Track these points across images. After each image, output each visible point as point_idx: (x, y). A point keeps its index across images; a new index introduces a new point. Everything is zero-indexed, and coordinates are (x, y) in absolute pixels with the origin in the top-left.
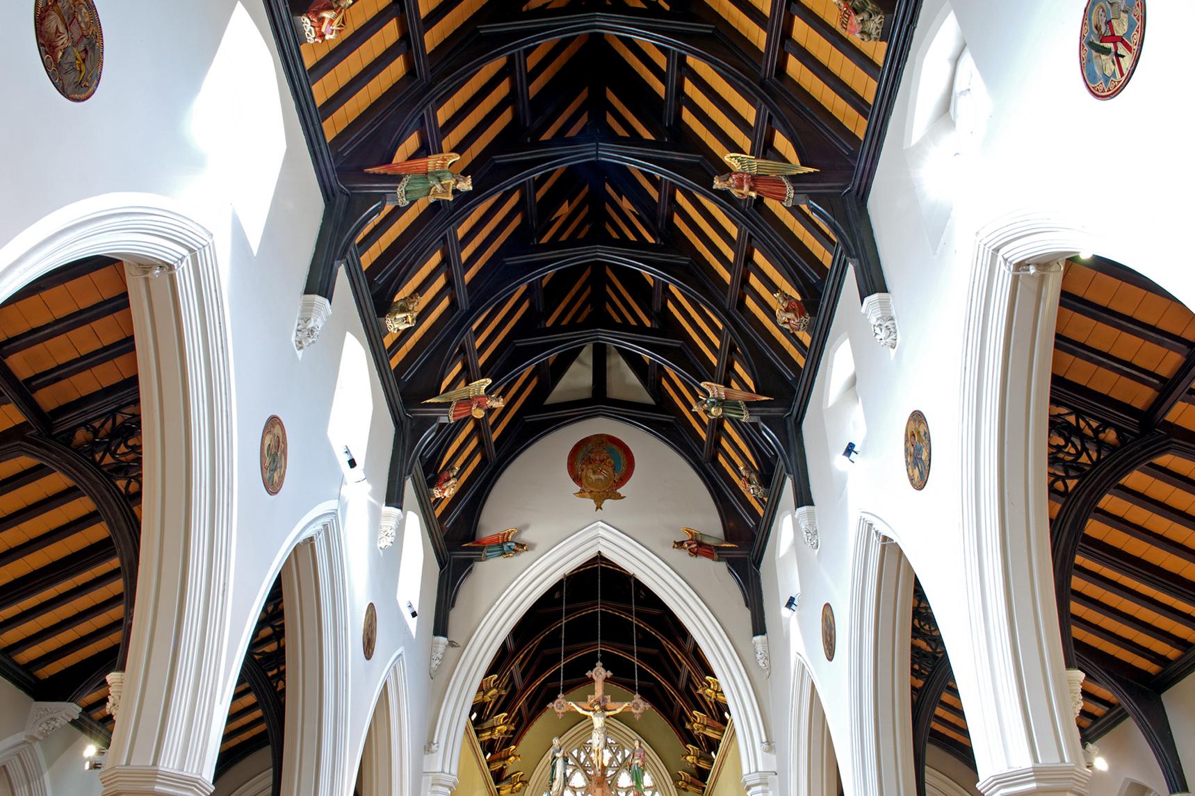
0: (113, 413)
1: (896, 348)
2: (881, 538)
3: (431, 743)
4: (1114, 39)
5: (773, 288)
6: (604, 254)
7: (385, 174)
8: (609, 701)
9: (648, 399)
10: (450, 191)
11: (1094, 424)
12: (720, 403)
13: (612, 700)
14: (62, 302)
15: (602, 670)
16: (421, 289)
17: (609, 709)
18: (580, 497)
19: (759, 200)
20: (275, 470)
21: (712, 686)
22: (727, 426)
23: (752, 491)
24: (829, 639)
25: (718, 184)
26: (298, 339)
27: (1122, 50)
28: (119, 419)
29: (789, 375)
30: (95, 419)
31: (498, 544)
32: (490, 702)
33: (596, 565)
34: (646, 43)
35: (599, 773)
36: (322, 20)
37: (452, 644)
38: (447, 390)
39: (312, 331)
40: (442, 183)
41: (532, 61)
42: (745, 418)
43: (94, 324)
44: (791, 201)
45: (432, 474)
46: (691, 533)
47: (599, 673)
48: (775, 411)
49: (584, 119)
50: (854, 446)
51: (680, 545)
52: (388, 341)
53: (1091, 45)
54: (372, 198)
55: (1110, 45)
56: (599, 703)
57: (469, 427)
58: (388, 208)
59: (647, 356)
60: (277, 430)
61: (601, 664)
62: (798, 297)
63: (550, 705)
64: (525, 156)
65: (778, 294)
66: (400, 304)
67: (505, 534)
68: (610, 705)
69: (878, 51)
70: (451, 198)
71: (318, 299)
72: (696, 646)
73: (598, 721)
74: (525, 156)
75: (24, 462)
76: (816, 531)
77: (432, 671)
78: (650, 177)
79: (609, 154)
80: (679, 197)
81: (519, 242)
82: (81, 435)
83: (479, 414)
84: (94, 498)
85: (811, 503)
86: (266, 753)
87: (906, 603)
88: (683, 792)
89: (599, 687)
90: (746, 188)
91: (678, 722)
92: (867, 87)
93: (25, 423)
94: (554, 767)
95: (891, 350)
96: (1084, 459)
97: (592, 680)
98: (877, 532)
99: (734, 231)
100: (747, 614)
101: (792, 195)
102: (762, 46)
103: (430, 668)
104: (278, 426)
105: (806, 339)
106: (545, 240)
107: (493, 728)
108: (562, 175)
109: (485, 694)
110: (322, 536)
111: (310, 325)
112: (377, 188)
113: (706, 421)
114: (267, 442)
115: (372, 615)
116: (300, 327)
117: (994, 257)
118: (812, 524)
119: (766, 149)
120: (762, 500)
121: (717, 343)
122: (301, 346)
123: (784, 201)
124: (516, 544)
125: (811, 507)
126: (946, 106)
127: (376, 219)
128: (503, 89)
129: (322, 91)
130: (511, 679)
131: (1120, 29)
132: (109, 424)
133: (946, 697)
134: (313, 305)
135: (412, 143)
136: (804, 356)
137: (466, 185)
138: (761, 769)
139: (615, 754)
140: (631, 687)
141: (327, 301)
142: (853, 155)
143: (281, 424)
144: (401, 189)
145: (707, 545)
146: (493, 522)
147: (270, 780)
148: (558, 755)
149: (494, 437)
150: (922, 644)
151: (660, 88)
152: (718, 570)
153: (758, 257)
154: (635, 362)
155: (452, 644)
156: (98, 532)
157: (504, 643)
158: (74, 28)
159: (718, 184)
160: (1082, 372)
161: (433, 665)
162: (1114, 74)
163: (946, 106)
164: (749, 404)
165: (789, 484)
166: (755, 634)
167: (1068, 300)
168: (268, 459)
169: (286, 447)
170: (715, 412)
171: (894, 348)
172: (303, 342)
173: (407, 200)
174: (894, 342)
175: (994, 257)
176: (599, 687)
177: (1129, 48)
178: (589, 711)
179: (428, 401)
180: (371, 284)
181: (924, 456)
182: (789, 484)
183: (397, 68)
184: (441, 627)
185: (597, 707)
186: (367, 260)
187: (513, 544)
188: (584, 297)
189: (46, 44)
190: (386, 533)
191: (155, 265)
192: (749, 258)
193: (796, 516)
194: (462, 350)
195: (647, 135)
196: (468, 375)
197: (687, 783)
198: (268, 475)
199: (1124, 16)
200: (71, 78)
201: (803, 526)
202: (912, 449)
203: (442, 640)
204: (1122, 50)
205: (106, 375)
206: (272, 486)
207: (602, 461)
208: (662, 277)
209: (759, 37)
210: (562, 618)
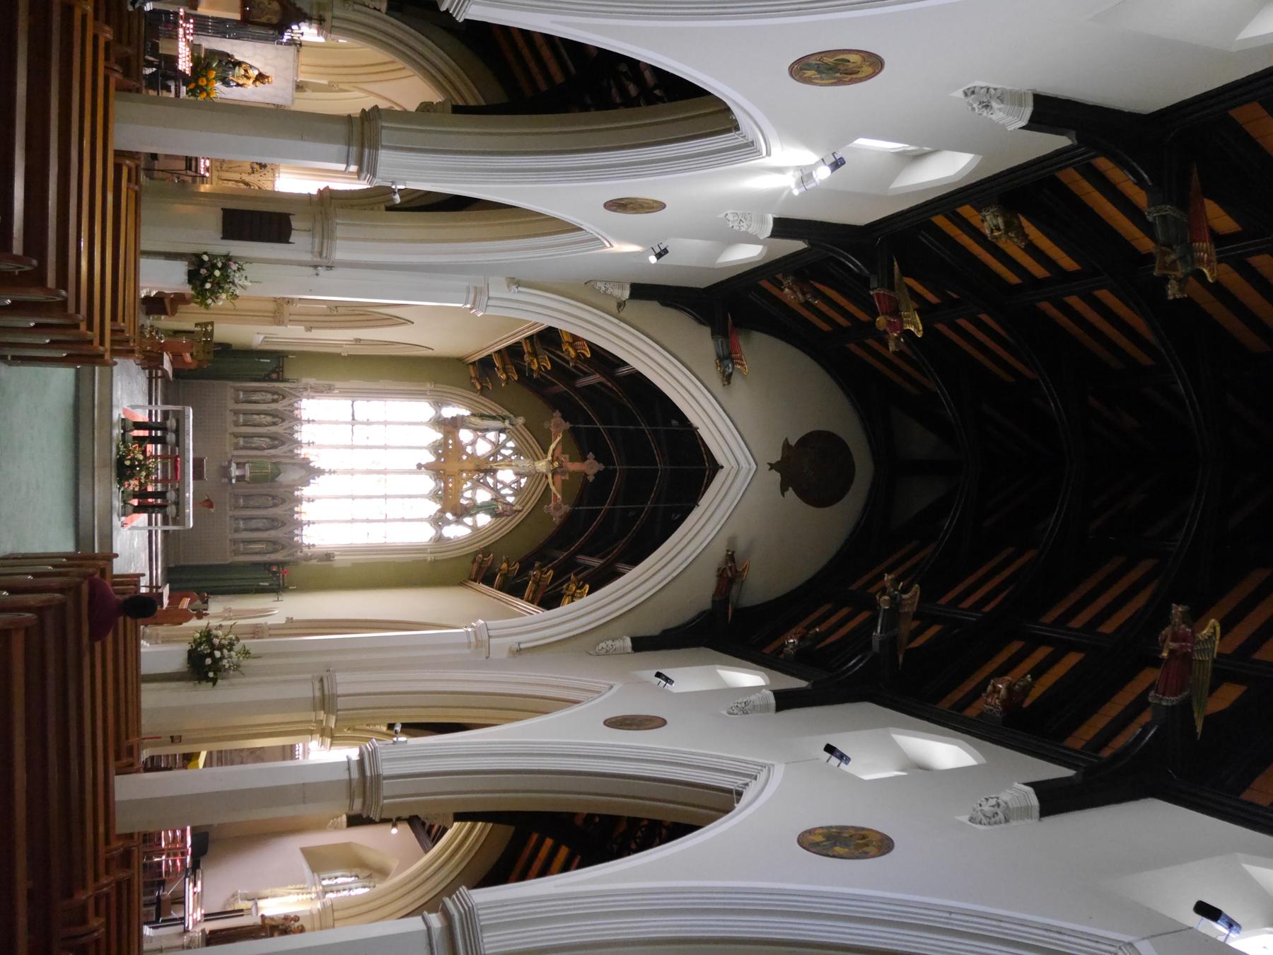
1: (969, 823)
2: (740, 789)
3: (519, 284)
5: (1038, 672)
8: (563, 478)
10: (1166, 272)
13: (563, 481)
15: (595, 470)
16: (1032, 249)
17: (555, 477)
18: (784, 445)
19: (1156, 662)
20: (819, 72)
21: (578, 591)
22: (865, 615)
24: (628, 722)
25: (1178, 610)
26: (976, 90)
31: (730, 354)
32: (563, 352)
33: (707, 465)
35: (489, 467)
37: (621, 305)
39: (987, 106)
40: (1178, 262)
44: (1158, 702)
46: (743, 570)
47: (591, 467)
50: (846, 764)
51: (731, 557)
52: (967, 211)
56: (561, 466)
57: (863, 316)
60: (867, 70)
61: (602, 469)
62: (1028, 702)
63: (557, 414)
65: (1030, 680)
66: (1016, 222)
67: (742, 360)
68: (559, 478)
71: (1028, 111)
72: (621, 574)
73: (542, 466)
76: (747, 713)
77: (592, 283)
83: (881, 321)
86: (499, 96)
87: (670, 812)
88: (471, 558)
89: (576, 466)
90: (1173, 645)
91: (539, 555)
94: (494, 418)
95: (967, 817)
97: (584, 459)
98: (747, 784)
99: (1108, 628)
101: (1164, 704)
103: (596, 281)
104: (870, 70)
105: (971, 712)
107: (534, 354)
109: (571, 344)
110: (741, 141)
111: (995, 105)
113: (871, 590)
115: (653, 208)
116: (992, 91)
119: (1223, 673)
120: (782, 652)
122: (969, 93)
123: (1156, 692)
124: (731, 374)
125: (228, 207)
130: (586, 374)
133: (564, 852)
134: (1020, 105)
138: (492, 641)
139: (509, 486)
140: (580, 501)
141: (1024, 123)
145: (731, 588)
147: (472, 103)
148: (507, 422)
150: (623, 827)
152: (701, 595)
153: (1072, 659)
155: (621, 305)
157: (625, 364)
159: (1178, 610)
161: (599, 284)
165: (800, 684)
166: (634, 640)
168: (832, 60)
169: (845, 83)
170: (884, 602)
171: (970, 821)
172: (973, 96)
173: (1154, 218)
174: (978, 821)
178: (552, 456)
179: (896, 263)
181: (838, 849)
182: (800, 684)
184: (641, 291)
185: (556, 464)
186: (1072, 179)
187: (730, 370)
190: (743, 219)
192: (1070, 647)
193: (764, 690)
196: (926, 311)
197: (481, 563)
198: (813, 61)
203: (627, 294)
210: (650, 426)
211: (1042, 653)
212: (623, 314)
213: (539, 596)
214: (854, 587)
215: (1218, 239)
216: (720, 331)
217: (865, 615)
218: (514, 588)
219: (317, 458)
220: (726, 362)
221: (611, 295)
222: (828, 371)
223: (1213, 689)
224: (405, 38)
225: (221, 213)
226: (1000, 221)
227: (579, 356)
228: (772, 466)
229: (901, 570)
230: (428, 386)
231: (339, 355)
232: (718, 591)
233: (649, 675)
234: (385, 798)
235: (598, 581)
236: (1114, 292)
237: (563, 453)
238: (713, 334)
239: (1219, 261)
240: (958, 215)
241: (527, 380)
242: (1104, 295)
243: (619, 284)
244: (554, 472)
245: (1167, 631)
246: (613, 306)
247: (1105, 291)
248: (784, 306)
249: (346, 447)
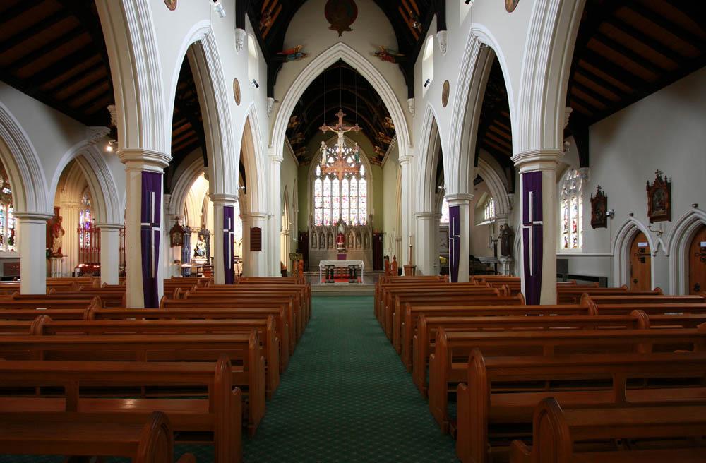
3: (270, 143)
37: (276, 101)
51: (378, 54)
71: (241, 30)
73: (341, 135)
86: (199, 150)
89: (341, 121)
107: (296, 139)
110: (205, 40)
117: (475, 40)
118: (444, 40)
146: (292, 39)
147: (203, 161)
152: (392, 68)
155: (276, 101)
176: (341, 121)
184: (270, 93)
203: (271, 99)
206: (238, 103)
212: (280, 100)
213: (389, 138)
218: (385, 147)
219: (336, 217)
222: (297, 9)
224: (181, 185)
225: (252, 252)
227: (297, 120)
228: (340, 35)
230: (309, 181)
231: (299, 213)
233: (425, 90)
234: (554, 147)
235: (384, 113)
237: (335, 126)
238: (286, 62)
241: (305, 143)
243: (267, 103)
244: (343, 130)
246: (277, 104)
248: (273, 27)
249: (332, 211)
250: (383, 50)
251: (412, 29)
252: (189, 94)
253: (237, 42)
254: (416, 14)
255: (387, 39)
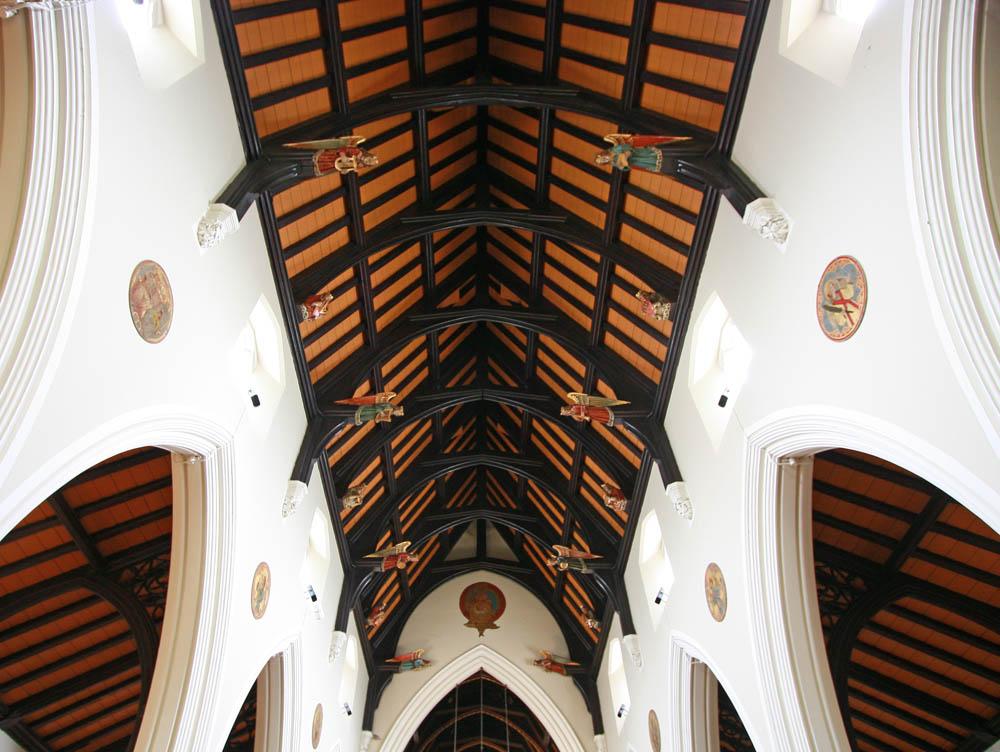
0: (150, 560)
4: (843, 301)
5: (600, 482)
6: (483, 460)
7: (348, 405)
9: (514, 558)
11: (846, 575)
12: (565, 559)
14: (124, 480)
16: (367, 481)
22: (570, 577)
23: (589, 623)
27: (850, 307)
28: (155, 563)
29: (613, 541)
30: (136, 564)
34: (511, 326)
36: (314, 307)
37: (375, 737)
38: (380, 549)
41: (442, 339)
42: (584, 570)
43: (146, 496)
45: (366, 610)
48: (605, 566)
49: (474, 375)
51: (539, 663)
52: (343, 515)
53: (826, 307)
54: (343, 419)
55: (841, 306)
58: (349, 427)
59: (514, 528)
60: (265, 573)
62: (617, 487)
64: (436, 397)
69: (667, 329)
70: (390, 420)
74: (436, 397)
75: (81, 593)
78: (515, 411)
79: (491, 396)
80: (535, 424)
81: (432, 452)
82: (127, 574)
83: (401, 565)
84: (129, 621)
85: (634, 632)
90: (582, 414)
92: (660, 350)
93: (88, 565)
96: (841, 599)
99: (572, 445)
100: (589, 717)
102: (589, 328)
105: (625, 517)
106: (448, 451)
108: (460, 410)
110: (289, 652)
112: (343, 413)
114: (258, 578)
117: (762, 454)
118: (636, 649)
119: (593, 391)
121: (562, 519)
126: (718, 360)
127: (340, 434)
128: (423, 356)
129: (312, 351)
131: (848, 294)
132: (147, 567)
135: (365, 387)
136: (623, 527)
137: (400, 412)
142: (653, 394)
143: (268, 567)
144: (358, 414)
146: (409, 640)
149: (411, 582)
151: (522, 356)
152: (564, 684)
153: (589, 462)
154: (505, 532)
155: (375, 737)
156: (128, 646)
158: (155, 298)
159: (563, 412)
160: (834, 537)
162: (846, 324)
163: (718, 360)
164: (586, 561)
165: (616, 617)
167: (819, 486)
170: (564, 566)
175: (762, 454)
177: (856, 306)
180: (334, 476)
181: (722, 596)
182: (616, 617)
183: (358, 341)
184: (368, 724)
188: (471, 490)
189: (135, 305)
191: (192, 455)
192: (583, 463)
194: (391, 522)
195: (514, 385)
199: (850, 287)
200: (150, 327)
201: (630, 648)
202: (711, 592)
203: (368, 734)
204: (850, 307)
205: (149, 532)
206: (258, 612)
207: (484, 601)
208: (523, 474)
209: (587, 322)
211: (586, 477)
212: (380, 734)
214: (553, 584)
215: (372, 391)
216: (396, 668)
217: (570, 577)
220: (416, 664)
221: (369, 745)
223: (603, 396)
226: (352, 498)
229: (543, 557)
232: (559, 671)
233: (620, 722)
236: (372, 252)
238: (398, 672)
239: (383, 391)
240: (345, 519)
242: (394, 444)
243: (361, 739)
245: (575, 417)
246: (376, 743)
247: (377, 322)
248: (384, 625)
250: (546, 657)
251: (587, 629)
252: (245, 737)
253: (331, 650)
254: (589, 608)
255: (554, 643)
